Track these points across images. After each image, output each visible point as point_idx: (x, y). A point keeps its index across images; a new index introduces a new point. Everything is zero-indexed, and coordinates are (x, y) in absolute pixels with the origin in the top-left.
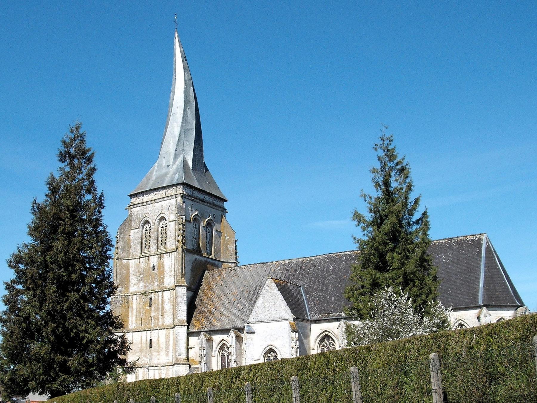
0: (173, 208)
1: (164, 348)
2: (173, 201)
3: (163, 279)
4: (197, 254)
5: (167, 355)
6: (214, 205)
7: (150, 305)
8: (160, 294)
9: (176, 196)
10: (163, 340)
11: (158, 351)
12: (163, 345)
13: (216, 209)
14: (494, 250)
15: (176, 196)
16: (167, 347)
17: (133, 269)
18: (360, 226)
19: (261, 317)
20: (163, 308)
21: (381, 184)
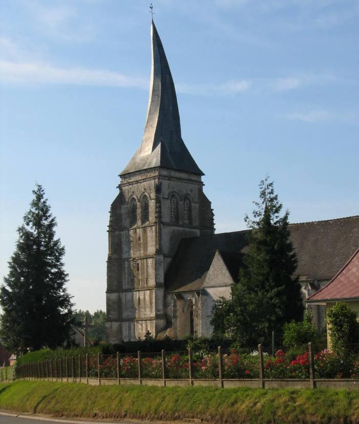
0: (153, 187)
1: (149, 305)
2: (153, 182)
3: (147, 248)
4: (176, 226)
5: (151, 311)
6: (191, 180)
7: (138, 270)
8: (145, 260)
9: (154, 178)
10: (147, 298)
11: (145, 308)
12: (148, 303)
13: (193, 184)
14: (333, 280)
15: (154, 178)
16: (151, 303)
17: (125, 239)
18: (280, 203)
19: (212, 283)
20: (147, 271)
21: (240, 283)
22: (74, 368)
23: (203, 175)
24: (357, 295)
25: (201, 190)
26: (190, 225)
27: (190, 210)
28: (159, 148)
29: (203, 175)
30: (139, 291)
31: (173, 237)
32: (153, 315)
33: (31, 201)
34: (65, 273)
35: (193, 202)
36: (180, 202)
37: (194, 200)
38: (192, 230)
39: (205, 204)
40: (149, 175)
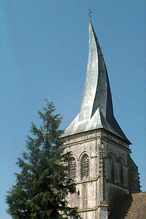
2: (94, 142)
9: (96, 138)
15: (96, 138)
22: (101, 206)
23: (131, 144)
24: (88, 218)
25: (129, 156)
26: (121, 184)
27: (121, 171)
28: (97, 112)
29: (131, 144)
30: (92, 181)
31: (111, 189)
32: (77, 187)
33: (29, 135)
34: (19, 171)
35: (124, 166)
36: (115, 163)
37: (125, 165)
38: (123, 189)
39: (133, 169)
40: (89, 136)
